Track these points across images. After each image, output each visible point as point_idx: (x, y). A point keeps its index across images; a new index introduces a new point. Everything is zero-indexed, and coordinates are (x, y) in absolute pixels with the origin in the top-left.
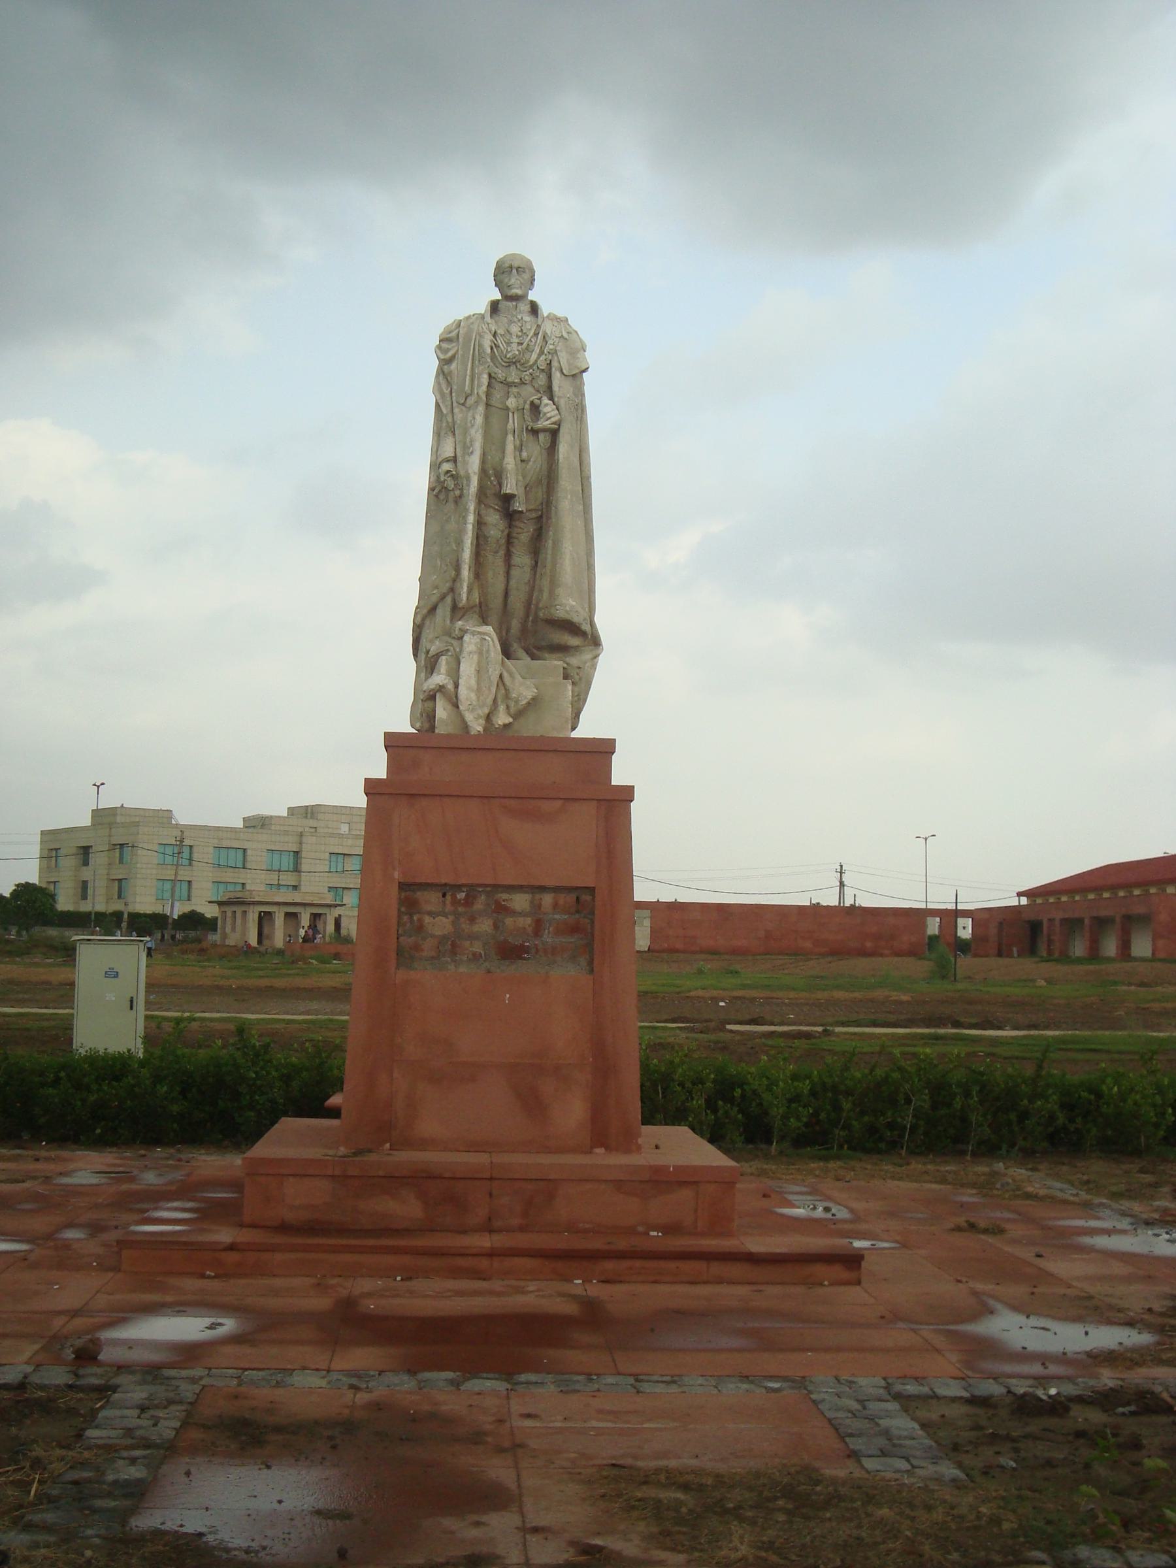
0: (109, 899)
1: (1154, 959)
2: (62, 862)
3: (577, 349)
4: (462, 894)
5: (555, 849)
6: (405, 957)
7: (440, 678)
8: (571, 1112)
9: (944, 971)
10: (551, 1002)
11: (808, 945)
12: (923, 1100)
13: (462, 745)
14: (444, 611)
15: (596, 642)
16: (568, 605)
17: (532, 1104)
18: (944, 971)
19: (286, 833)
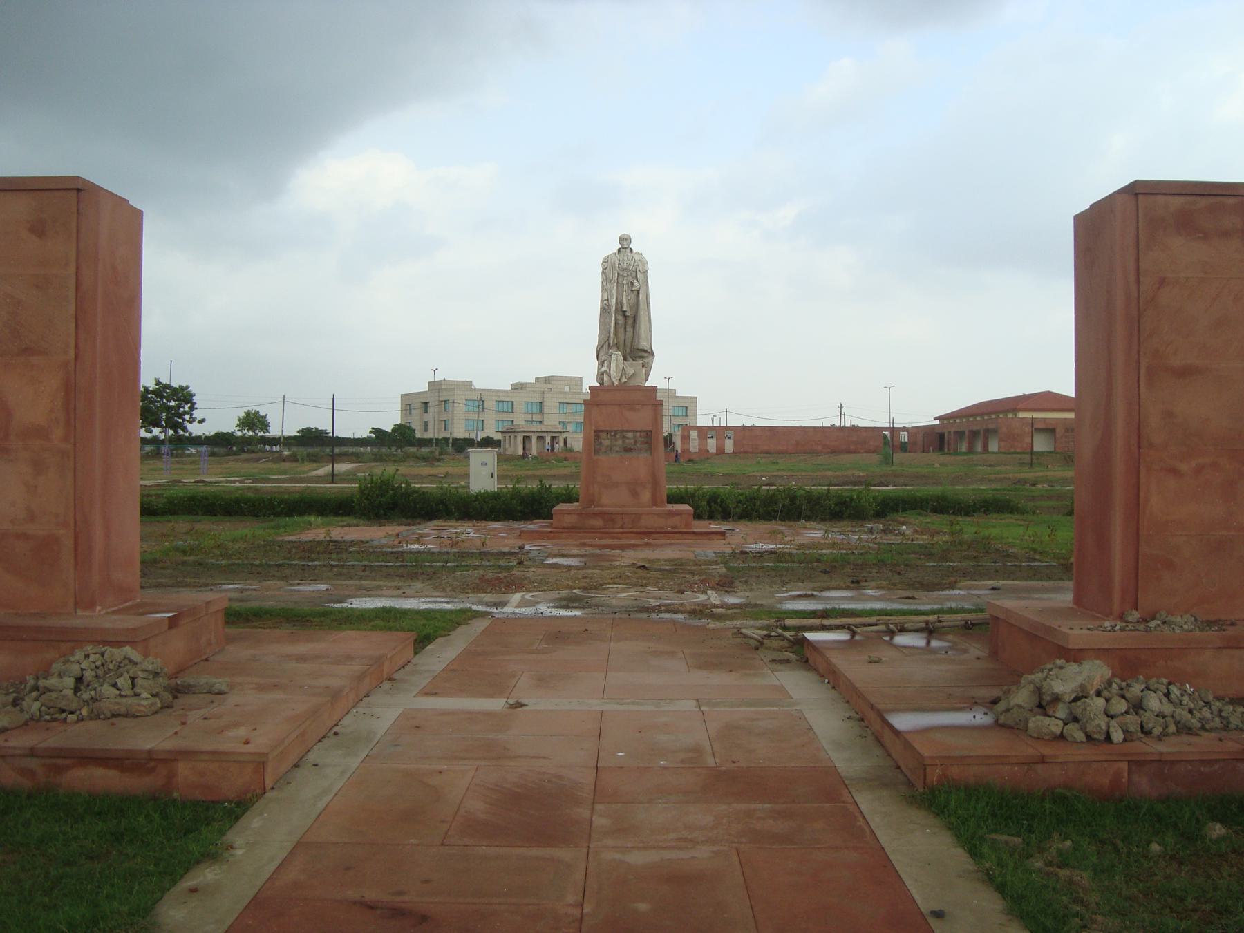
0: (439, 431)
1: (999, 452)
2: (413, 412)
3: (645, 263)
4: (612, 433)
5: (640, 419)
6: (596, 452)
7: (605, 368)
8: (646, 496)
9: (888, 461)
10: (639, 464)
11: (820, 448)
12: (787, 502)
13: (612, 389)
14: (606, 346)
15: (653, 354)
16: (643, 344)
17: (635, 494)
18: (888, 461)
19: (534, 392)
